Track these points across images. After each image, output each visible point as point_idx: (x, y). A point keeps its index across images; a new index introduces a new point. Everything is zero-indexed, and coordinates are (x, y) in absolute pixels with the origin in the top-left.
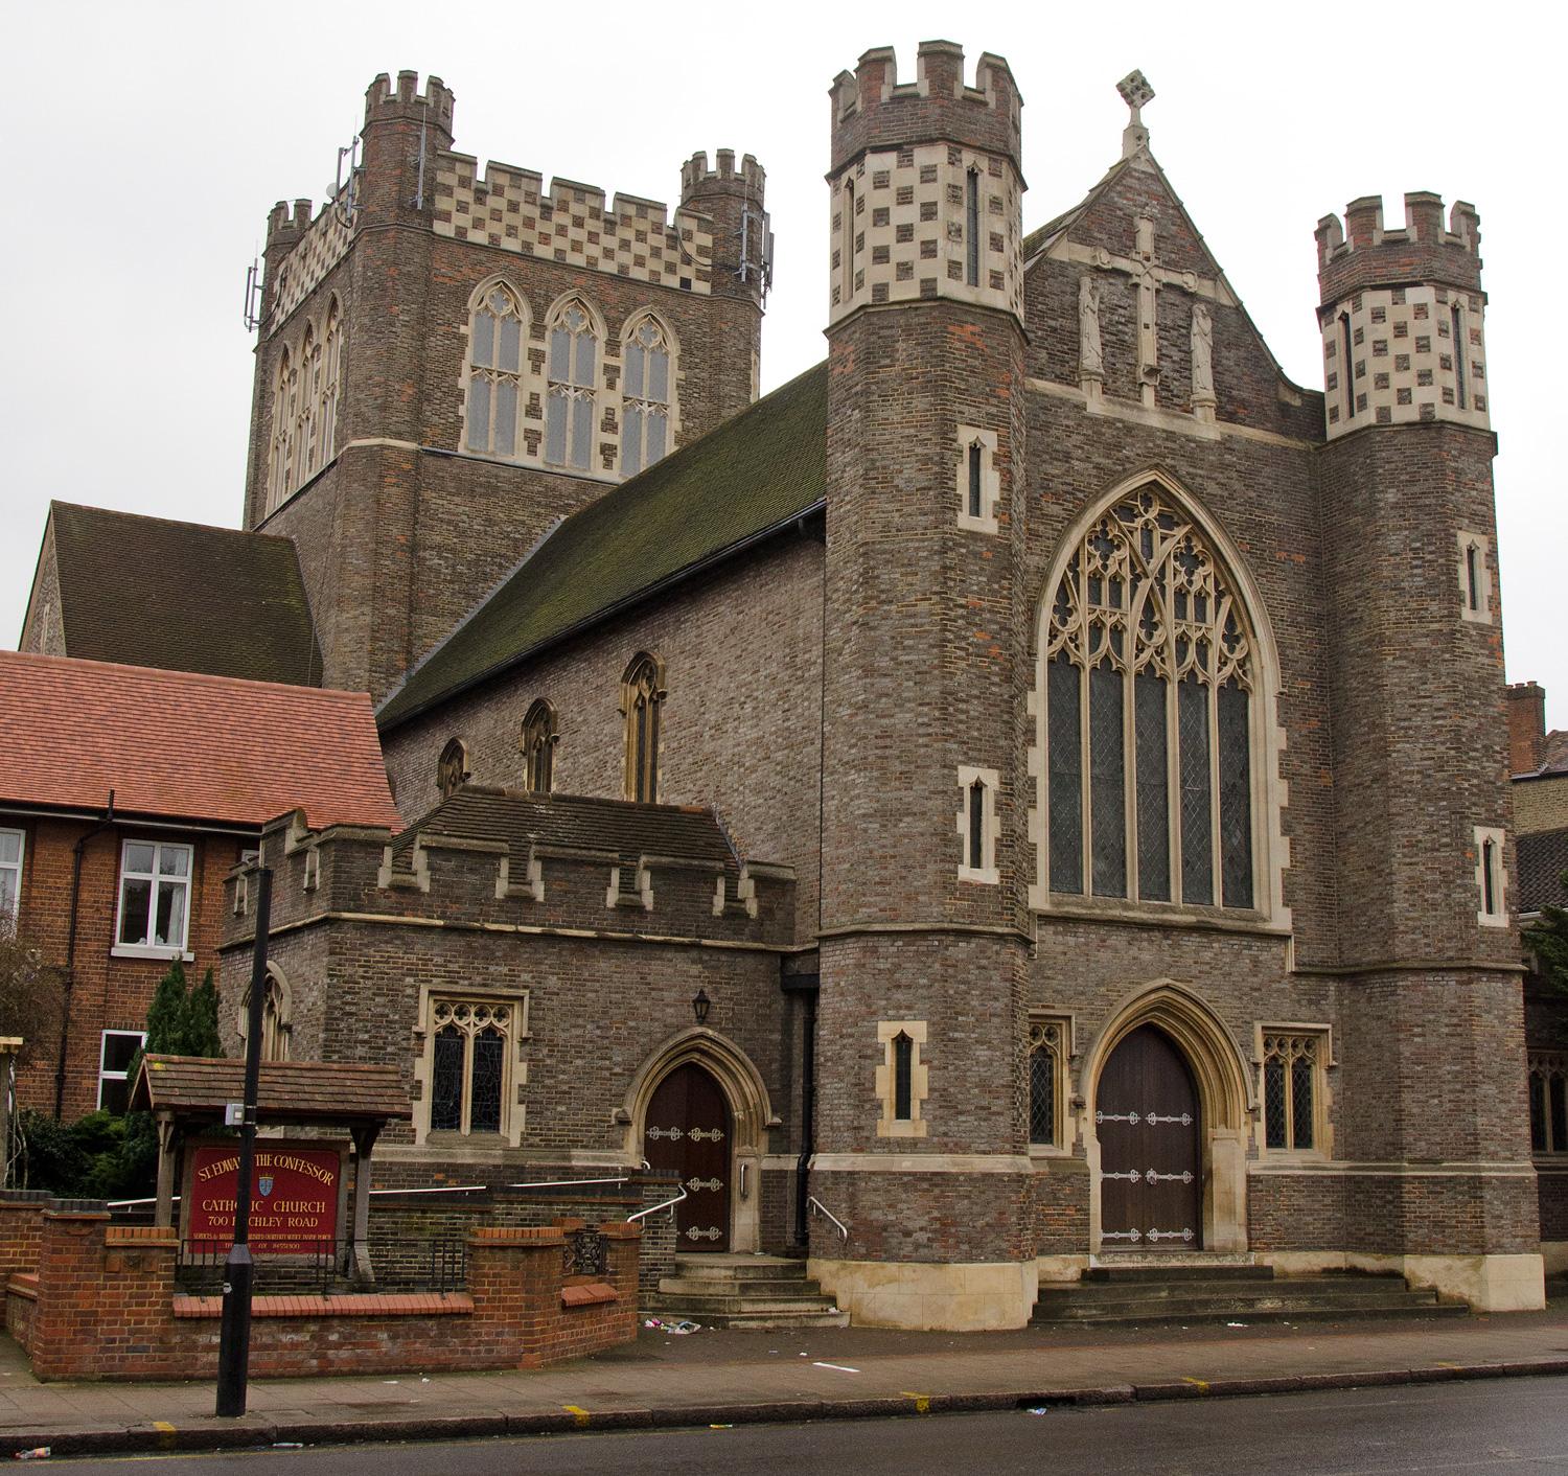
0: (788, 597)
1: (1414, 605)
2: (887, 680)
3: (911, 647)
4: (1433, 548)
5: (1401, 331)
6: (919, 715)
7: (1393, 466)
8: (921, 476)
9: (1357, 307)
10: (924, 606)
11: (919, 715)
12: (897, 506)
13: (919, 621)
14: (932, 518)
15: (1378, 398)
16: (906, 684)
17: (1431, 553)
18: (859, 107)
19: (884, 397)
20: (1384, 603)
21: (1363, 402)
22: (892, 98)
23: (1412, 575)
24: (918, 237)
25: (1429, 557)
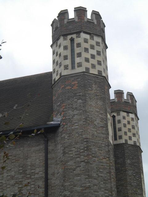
0: (32, 153)
1: (134, 190)
2: (96, 181)
3: (102, 172)
4: (138, 176)
5: (129, 123)
6: (105, 193)
7: (129, 154)
8: (101, 123)
9: (119, 114)
10: (104, 160)
11: (105, 193)
12: (96, 130)
13: (104, 164)
14: (105, 136)
15: (125, 137)
16: (101, 183)
17: (138, 177)
18: (59, 26)
19: (90, 99)
20: (128, 188)
21: (121, 137)
22: (67, 22)
23: (134, 182)
24: (62, 67)
25: (137, 178)
